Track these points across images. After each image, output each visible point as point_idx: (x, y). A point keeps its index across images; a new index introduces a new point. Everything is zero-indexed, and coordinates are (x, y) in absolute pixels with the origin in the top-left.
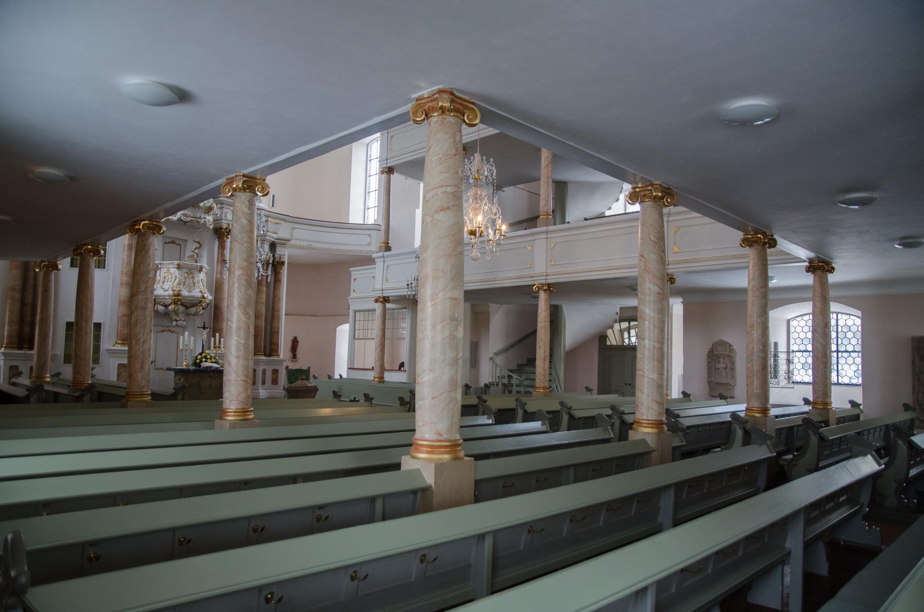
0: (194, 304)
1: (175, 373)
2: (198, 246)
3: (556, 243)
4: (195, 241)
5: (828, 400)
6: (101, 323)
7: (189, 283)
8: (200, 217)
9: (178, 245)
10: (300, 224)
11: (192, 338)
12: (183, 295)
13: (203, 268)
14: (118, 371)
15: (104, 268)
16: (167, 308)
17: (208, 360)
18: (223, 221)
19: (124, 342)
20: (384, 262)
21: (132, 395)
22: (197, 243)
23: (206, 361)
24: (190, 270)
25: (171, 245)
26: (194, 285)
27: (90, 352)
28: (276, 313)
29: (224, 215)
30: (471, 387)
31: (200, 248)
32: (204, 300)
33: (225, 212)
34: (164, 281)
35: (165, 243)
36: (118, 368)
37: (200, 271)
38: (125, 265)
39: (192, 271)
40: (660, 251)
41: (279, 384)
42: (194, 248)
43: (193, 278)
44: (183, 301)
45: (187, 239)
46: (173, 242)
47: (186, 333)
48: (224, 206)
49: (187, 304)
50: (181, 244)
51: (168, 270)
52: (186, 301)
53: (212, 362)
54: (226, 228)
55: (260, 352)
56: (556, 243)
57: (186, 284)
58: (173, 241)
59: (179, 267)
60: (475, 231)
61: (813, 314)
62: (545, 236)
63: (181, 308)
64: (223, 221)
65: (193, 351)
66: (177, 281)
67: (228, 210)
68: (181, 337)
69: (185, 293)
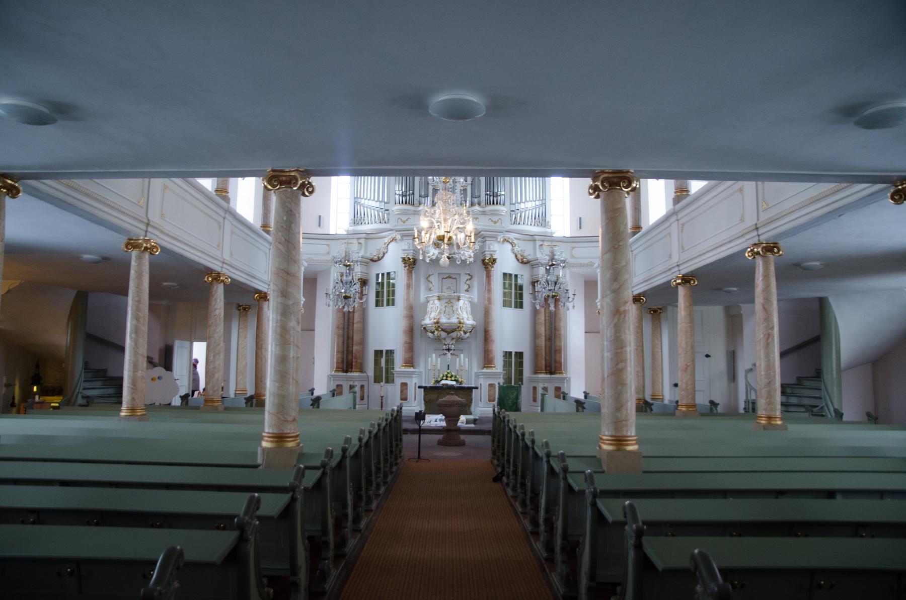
0: (454, 329)
1: (424, 391)
2: (469, 277)
4: (466, 274)
5: (625, 433)
7: (449, 312)
9: (454, 279)
10: (579, 242)
12: (442, 322)
17: (449, 378)
18: (486, 253)
23: (446, 379)
24: (449, 301)
26: (453, 312)
27: (832, 370)
28: (557, 332)
30: (718, 404)
31: (470, 279)
32: (461, 325)
34: (431, 312)
35: (443, 279)
36: (401, 386)
37: (459, 299)
38: (405, 301)
39: (452, 301)
40: (277, 243)
41: (408, 400)
42: (465, 280)
43: (452, 306)
44: (443, 327)
45: (459, 272)
46: (450, 277)
47: (462, 355)
50: (457, 277)
51: (434, 302)
53: (451, 380)
54: (490, 258)
57: (446, 312)
59: (439, 299)
60: (444, 236)
63: (443, 334)
64: (486, 253)
66: (439, 310)
68: (429, 359)
69: (444, 320)
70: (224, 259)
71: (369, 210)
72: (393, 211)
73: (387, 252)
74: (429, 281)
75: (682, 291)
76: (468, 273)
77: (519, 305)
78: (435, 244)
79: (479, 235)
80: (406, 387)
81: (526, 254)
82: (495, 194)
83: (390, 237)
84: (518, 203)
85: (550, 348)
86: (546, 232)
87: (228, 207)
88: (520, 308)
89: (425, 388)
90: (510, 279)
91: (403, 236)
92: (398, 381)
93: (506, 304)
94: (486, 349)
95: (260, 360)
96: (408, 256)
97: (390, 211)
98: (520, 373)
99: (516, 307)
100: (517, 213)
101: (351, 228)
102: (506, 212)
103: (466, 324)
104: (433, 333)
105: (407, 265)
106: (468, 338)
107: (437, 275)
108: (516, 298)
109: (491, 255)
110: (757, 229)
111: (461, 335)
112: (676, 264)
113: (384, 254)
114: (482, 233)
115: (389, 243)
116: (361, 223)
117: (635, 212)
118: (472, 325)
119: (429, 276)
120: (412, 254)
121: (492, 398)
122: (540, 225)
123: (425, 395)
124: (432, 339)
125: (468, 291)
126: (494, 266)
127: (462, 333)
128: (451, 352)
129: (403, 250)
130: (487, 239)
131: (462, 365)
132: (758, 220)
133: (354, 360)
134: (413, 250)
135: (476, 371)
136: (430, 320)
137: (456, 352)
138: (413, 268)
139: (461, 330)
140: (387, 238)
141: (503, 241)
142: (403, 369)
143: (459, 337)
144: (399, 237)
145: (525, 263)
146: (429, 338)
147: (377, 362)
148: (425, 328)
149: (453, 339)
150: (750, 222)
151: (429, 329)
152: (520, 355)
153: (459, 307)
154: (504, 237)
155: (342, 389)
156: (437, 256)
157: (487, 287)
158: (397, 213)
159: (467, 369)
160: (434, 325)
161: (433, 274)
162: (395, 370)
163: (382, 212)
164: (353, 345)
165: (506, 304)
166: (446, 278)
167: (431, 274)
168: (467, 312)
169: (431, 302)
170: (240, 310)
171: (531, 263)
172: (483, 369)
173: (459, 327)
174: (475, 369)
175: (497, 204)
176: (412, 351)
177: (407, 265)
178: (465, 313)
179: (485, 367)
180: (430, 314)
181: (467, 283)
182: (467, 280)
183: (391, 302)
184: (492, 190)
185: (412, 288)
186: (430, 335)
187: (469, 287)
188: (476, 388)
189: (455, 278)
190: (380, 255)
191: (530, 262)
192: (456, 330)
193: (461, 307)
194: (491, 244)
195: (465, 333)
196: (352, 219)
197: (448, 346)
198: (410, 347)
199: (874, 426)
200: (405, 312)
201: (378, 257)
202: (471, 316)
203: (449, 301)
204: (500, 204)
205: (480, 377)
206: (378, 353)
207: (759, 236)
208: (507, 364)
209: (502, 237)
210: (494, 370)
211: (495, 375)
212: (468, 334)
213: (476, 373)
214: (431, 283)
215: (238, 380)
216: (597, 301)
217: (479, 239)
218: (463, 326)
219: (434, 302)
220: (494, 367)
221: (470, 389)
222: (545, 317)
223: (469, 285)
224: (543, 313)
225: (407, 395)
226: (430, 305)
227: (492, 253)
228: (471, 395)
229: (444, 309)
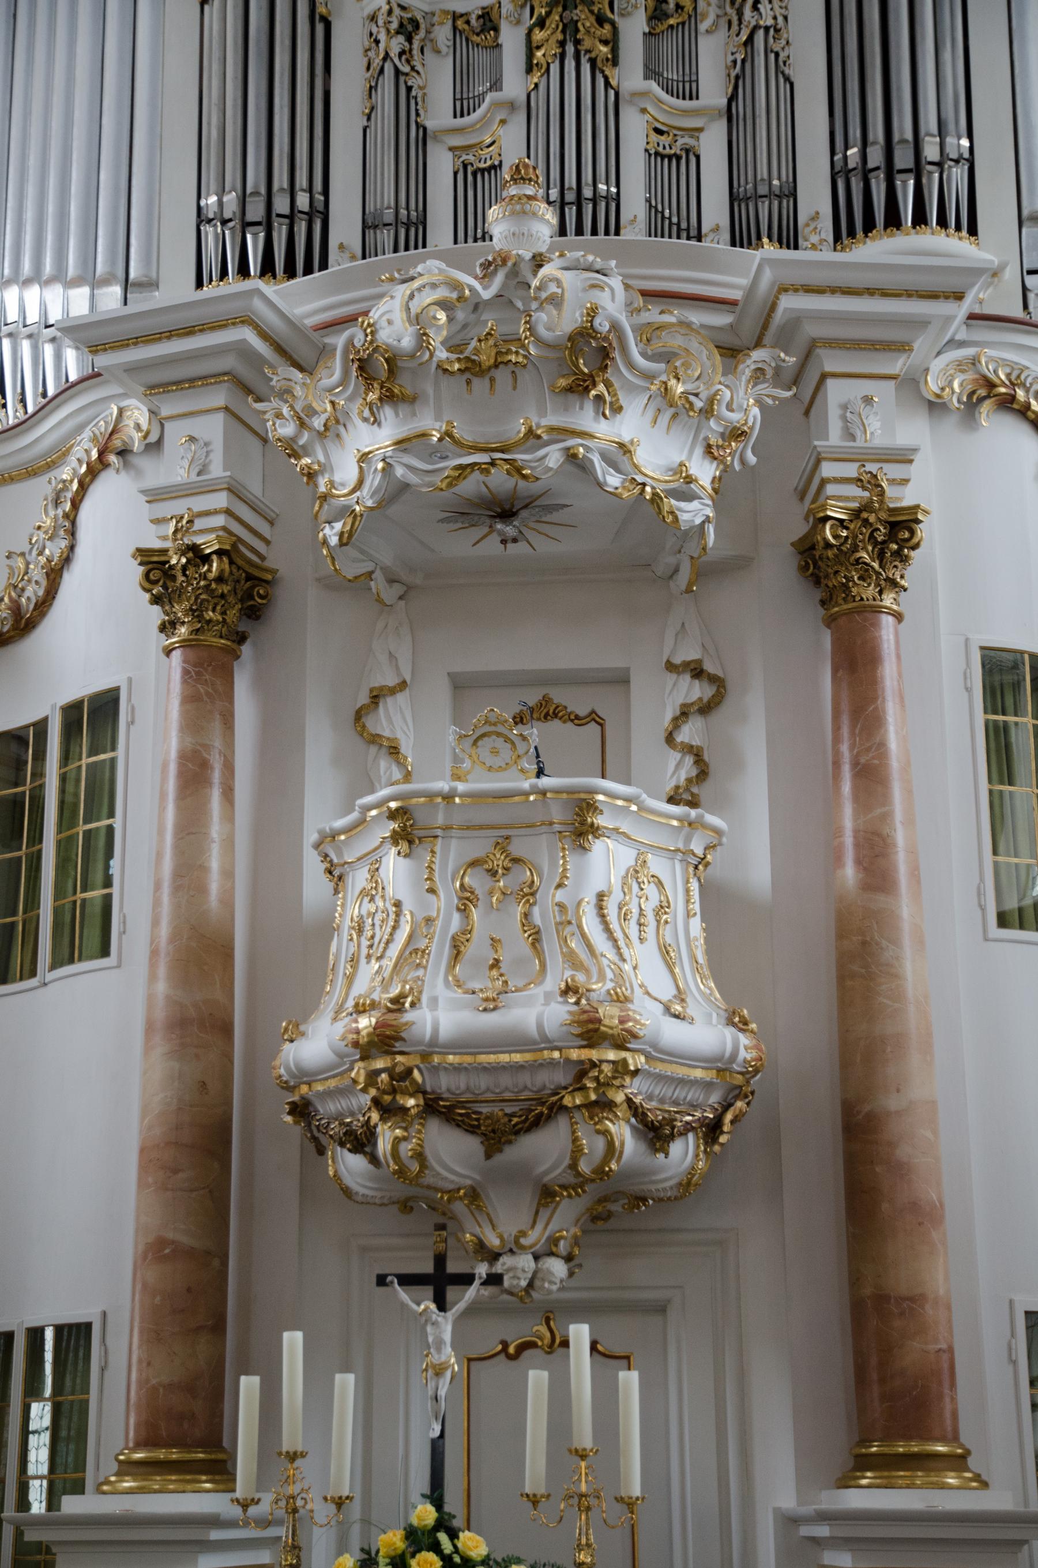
2: (697, 691)
6: (88, 1326)
8: (530, 432)
9: (577, 720)
11: (346, 1383)
15: (105, 952)
16: (374, 1160)
18: (828, 470)
19: (161, 1454)
24: (502, 844)
26: (536, 938)
31: (706, 709)
33: (845, 407)
34: (354, 961)
39: (517, 848)
42: (669, 716)
43: (529, 894)
44: (444, 1084)
45: (611, 660)
48: (828, 368)
49: (485, 1109)
52: (482, 1082)
54: (856, 514)
57: (477, 948)
58: (546, 700)
64: (828, 470)
65: (355, 1510)
68: (249, 1385)
71: (26, 346)
73: (67, 560)
74: (374, 739)
76: (689, 653)
78: (364, 366)
82: (903, 159)
94: (867, 1291)
103: (657, 1053)
105: (179, 610)
106: (687, 1185)
107: (441, 694)
109: (872, 483)
111: (611, 1150)
113: (55, 575)
115: (84, 487)
118: (721, 1065)
119: (376, 697)
120: (220, 521)
124: (366, 1202)
126: (911, 575)
130: (831, 361)
131: (585, 1437)
134: (234, 490)
135: (787, 1500)
139: (609, 1105)
141: (972, 404)
146: (347, 1192)
148: (302, 1110)
153: (589, 899)
154: (975, 361)
156: (388, 468)
157: (845, 748)
159: (636, 1491)
160: (359, 1072)
161: (403, 685)
167: (391, 681)
168: (665, 951)
169: (359, 879)
172: (845, 1482)
173: (583, 1070)
179: (863, 1463)
181: (686, 734)
182: (684, 714)
184: (877, 131)
185: (228, 793)
187: (703, 773)
189: (594, 717)
190: (30, 591)
193: (601, 897)
194: (868, 400)
199: (141, 1248)
201: (16, 610)
203: (502, 844)
204: (942, 222)
209: (960, 366)
213: (790, 1521)
214: (394, 751)
218: (621, 1069)
220: (959, 1462)
223: (697, 755)
229: (456, 921)
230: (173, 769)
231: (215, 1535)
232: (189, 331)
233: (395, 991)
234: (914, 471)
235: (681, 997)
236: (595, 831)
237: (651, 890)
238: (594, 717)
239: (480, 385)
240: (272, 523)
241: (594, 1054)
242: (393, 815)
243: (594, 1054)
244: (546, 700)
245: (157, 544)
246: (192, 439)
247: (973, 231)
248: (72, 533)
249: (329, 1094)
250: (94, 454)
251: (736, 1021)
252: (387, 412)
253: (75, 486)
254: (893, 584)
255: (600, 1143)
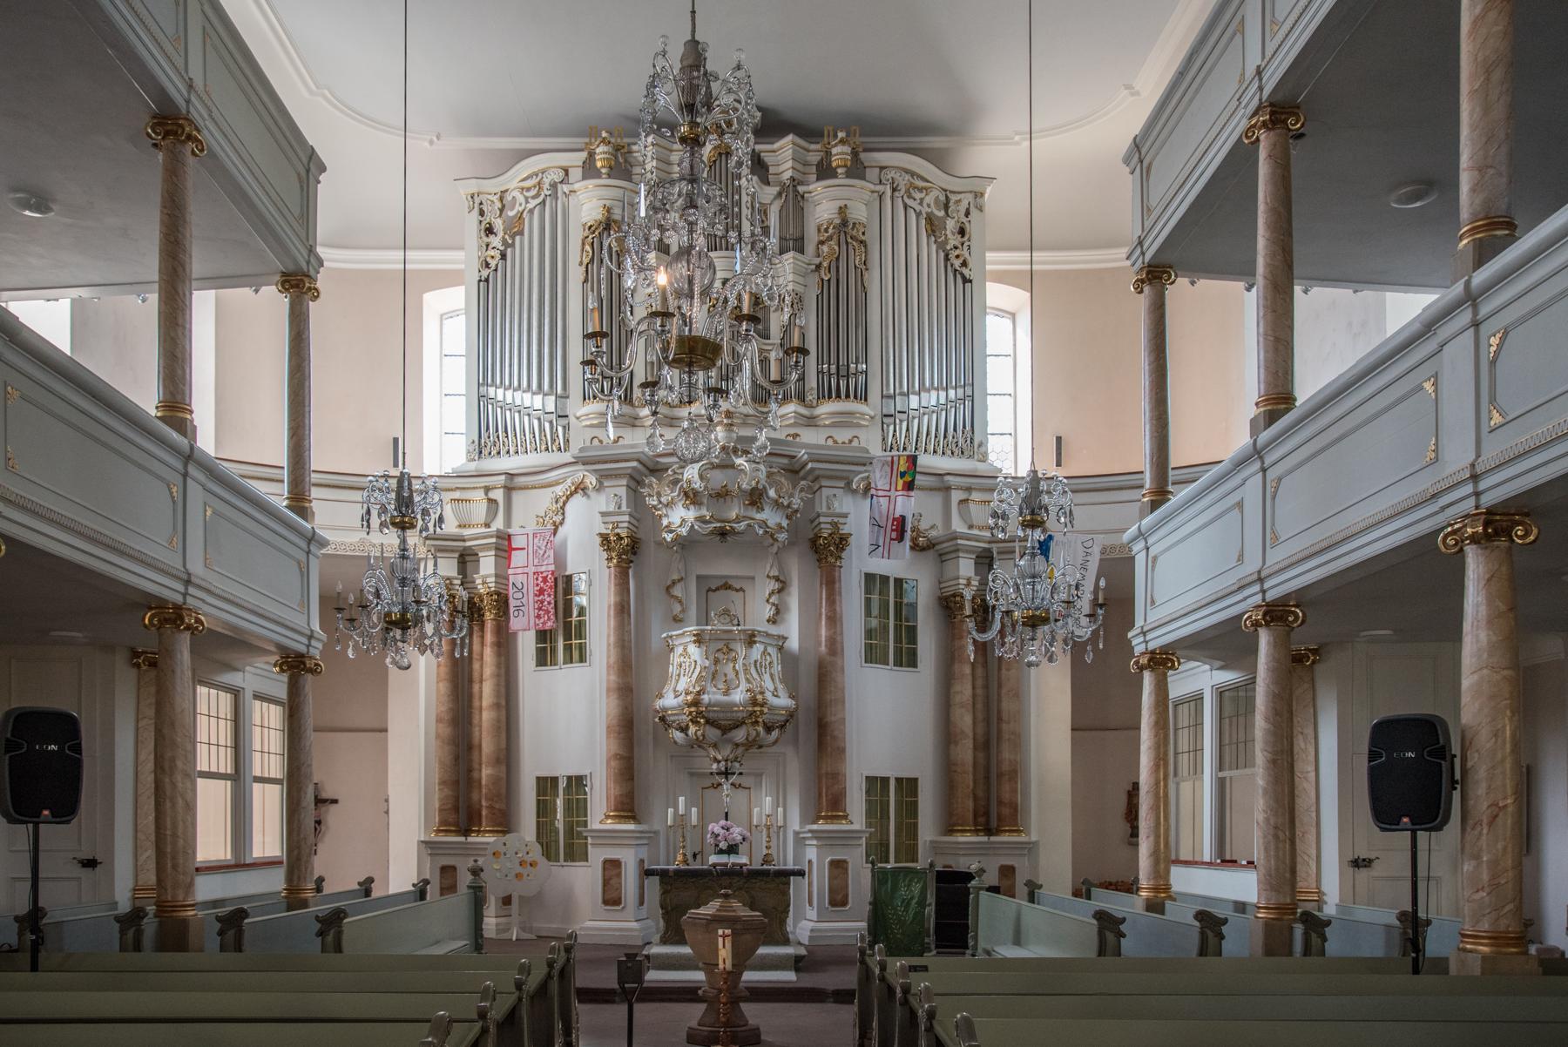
1: (662, 882)
3: (1506, 333)
9: (737, 590)
13: (754, 636)
14: (604, 876)
16: (687, 735)
18: (822, 519)
19: (622, 814)
20: (1148, 549)
21: (1272, 909)
22: (773, 582)
25: (722, 592)
29: (824, 504)
31: (780, 591)
33: (828, 497)
34: (679, 675)
36: (604, 869)
38: (612, 647)
39: (731, 646)
42: (767, 595)
45: (752, 574)
49: (723, 723)
51: (685, 650)
54: (830, 535)
55: (961, 826)
56: (1506, 333)
58: (726, 583)
59: (699, 640)
61: (160, 282)
62: (1465, 317)
64: (822, 519)
67: (835, 491)
70: (312, 631)
72: (578, 418)
75: (1475, 566)
77: (908, 658)
78: (686, 494)
79: (802, 473)
80: (614, 872)
81: (923, 526)
82: (843, 372)
83: (569, 481)
84: (902, 394)
85: (987, 769)
86: (976, 470)
87: (192, 448)
88: (909, 666)
89: (663, 874)
90: (883, 592)
91: (603, 476)
92: (597, 856)
93: (873, 655)
95: (168, 804)
96: (617, 531)
97: (572, 419)
98: (909, 829)
99: (898, 663)
100: (901, 421)
101: (473, 466)
102: (872, 418)
103: (772, 708)
104: (684, 730)
105: (614, 554)
106: (776, 742)
108: (898, 640)
109: (835, 525)
110: (1261, 580)
111: (758, 734)
112: (1255, 577)
114: (810, 465)
115: (568, 498)
116: (499, 453)
117: (1276, 350)
119: (674, 583)
120: (626, 525)
121: (839, 897)
122: (957, 451)
123: (665, 893)
124: (682, 745)
125: (774, 623)
126: (844, 555)
127: (760, 729)
128: (733, 779)
129: (603, 514)
132: (1145, 620)
133: (484, 803)
135: (797, 828)
136: (676, 697)
137: (744, 781)
138: (632, 562)
139: (757, 722)
140: (560, 487)
142: (610, 825)
143: (754, 740)
144: (591, 480)
145: (923, 549)
146: (675, 742)
147: (544, 810)
148: (662, 719)
149: (737, 745)
150: (1251, 566)
151: (674, 721)
152: (909, 786)
153: (752, 661)
154: (868, 477)
155: (455, 877)
156: (692, 526)
158: (588, 423)
160: (686, 710)
162: (589, 827)
163: (551, 422)
164: (480, 764)
165: (873, 655)
166: (717, 589)
168: (771, 675)
169: (680, 650)
170: (138, 666)
171: (937, 547)
172: (814, 822)
174: (795, 824)
175: (848, 396)
176: (633, 779)
177: (614, 554)
178: (767, 677)
180: (677, 681)
181: (773, 599)
183: (577, 654)
186: (678, 736)
187: (778, 612)
188: (801, 873)
191: (934, 545)
192: (744, 723)
194: (835, 495)
195: (769, 729)
196: (473, 442)
197: (723, 763)
198: (628, 769)
200: (613, 678)
202: (780, 687)
205: (807, 842)
206: (546, 785)
207: (1147, 642)
208: (876, 811)
209: (863, 479)
210: (843, 826)
211: (847, 838)
212: (775, 734)
213: (796, 833)
215: (139, 864)
216: (1130, 635)
217: (803, 483)
219: (685, 650)
220: (845, 817)
221: (785, 875)
222: (974, 688)
224: (970, 678)
225: (621, 893)
226: (676, 658)
227: (836, 520)
228: (786, 893)
230: (612, 608)
231: (638, 835)
232: (617, 461)
233: (698, 689)
234: (848, 520)
235: (776, 689)
236: (755, 642)
237: (768, 657)
238: (741, 590)
239: (721, 500)
240: (638, 521)
241: (756, 709)
242: (694, 635)
243: (756, 709)
244: (726, 583)
245: (605, 531)
246: (616, 495)
247: (866, 400)
248: (563, 514)
249: (672, 715)
250: (573, 488)
251: (792, 697)
252: (692, 507)
253: (564, 498)
254: (841, 558)
255: (754, 733)
